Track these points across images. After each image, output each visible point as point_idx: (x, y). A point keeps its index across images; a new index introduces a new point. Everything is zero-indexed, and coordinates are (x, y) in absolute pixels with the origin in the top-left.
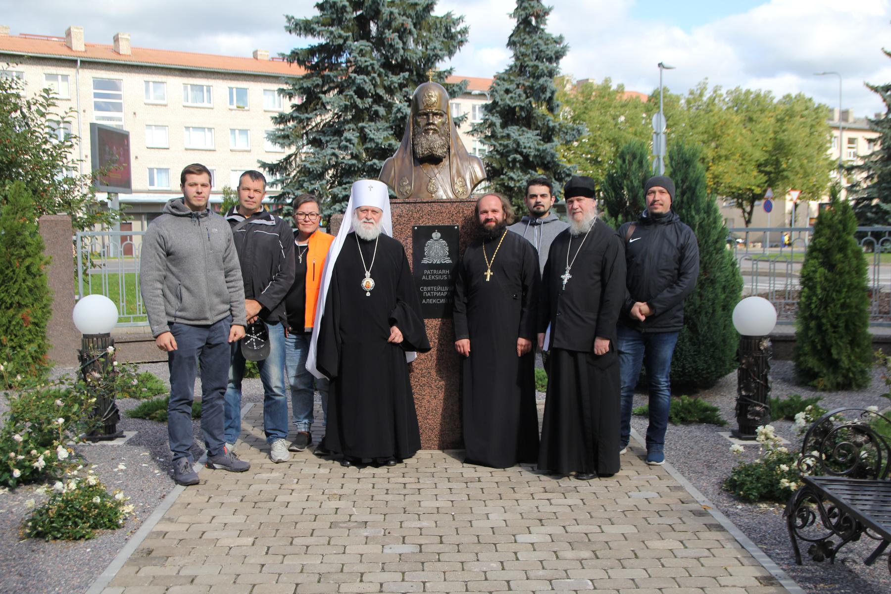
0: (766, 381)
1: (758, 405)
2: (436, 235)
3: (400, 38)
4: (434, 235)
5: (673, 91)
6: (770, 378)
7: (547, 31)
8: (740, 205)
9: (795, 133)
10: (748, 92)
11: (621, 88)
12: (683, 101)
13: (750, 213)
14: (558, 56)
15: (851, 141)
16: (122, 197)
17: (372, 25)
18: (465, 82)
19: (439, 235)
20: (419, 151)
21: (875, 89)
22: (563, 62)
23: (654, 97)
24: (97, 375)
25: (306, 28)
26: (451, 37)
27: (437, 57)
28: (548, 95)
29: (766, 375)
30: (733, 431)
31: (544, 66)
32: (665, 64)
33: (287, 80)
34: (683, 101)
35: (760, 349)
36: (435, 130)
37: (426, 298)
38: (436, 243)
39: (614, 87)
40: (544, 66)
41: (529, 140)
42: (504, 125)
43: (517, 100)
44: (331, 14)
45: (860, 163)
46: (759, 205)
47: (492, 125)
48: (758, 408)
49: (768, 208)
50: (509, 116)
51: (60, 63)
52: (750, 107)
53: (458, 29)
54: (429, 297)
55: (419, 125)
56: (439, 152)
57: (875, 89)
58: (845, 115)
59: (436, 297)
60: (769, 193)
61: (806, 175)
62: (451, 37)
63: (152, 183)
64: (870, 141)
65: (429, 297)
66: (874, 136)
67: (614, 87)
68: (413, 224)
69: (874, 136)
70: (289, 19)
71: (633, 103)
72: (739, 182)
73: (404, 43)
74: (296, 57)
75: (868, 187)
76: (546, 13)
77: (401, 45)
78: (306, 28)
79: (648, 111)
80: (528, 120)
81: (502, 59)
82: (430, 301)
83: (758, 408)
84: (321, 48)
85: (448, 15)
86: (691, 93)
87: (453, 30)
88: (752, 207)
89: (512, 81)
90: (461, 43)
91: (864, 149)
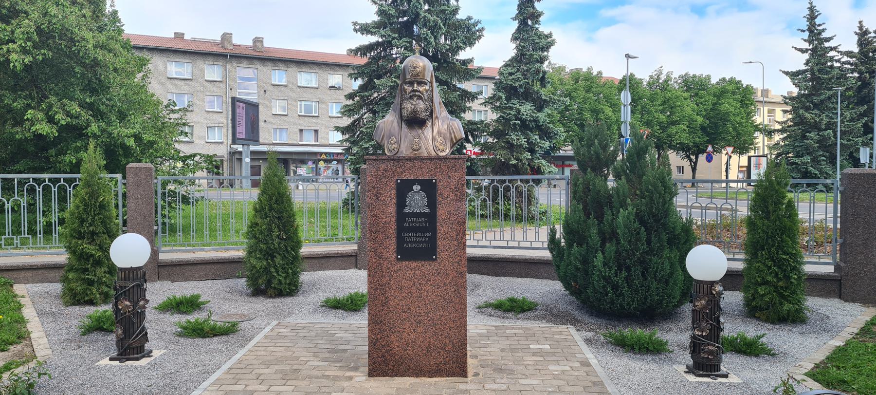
0: (719, 322)
1: (712, 345)
2: (416, 188)
3: (432, 33)
4: (414, 187)
5: (638, 76)
6: (722, 320)
7: (540, 30)
8: (688, 157)
9: (728, 106)
10: (694, 76)
11: (600, 73)
12: (645, 83)
13: (695, 163)
14: (547, 48)
15: (770, 111)
16: (253, 148)
17: (415, 27)
18: (480, 69)
19: (419, 187)
20: (405, 113)
21: (787, 73)
22: (552, 50)
23: (623, 81)
24: (128, 303)
25: (365, 29)
26: (469, 33)
27: (459, 48)
28: (541, 75)
29: (719, 317)
30: (687, 367)
31: (537, 55)
32: (631, 54)
33: (355, 67)
34: (645, 83)
35: (712, 293)
36: (419, 96)
37: (407, 242)
38: (417, 194)
39: (595, 73)
40: (537, 55)
41: (526, 109)
42: (508, 99)
43: (518, 80)
44: (385, 21)
45: (778, 127)
46: (702, 158)
47: (500, 98)
48: (711, 348)
49: (709, 159)
50: (511, 92)
51: (196, 57)
52: (694, 86)
53: (477, 28)
54: (410, 242)
55: (406, 92)
56: (423, 115)
57: (787, 73)
58: (765, 92)
59: (416, 242)
60: (710, 149)
61: (738, 135)
62: (469, 33)
63: (316, 140)
64: (785, 112)
65: (410, 242)
66: (789, 108)
67: (595, 73)
68: (396, 177)
69: (789, 108)
70: (355, 24)
71: (610, 82)
72: (685, 138)
73: (435, 38)
74: (363, 50)
75: (785, 145)
76: (539, 16)
77: (432, 40)
78: (365, 29)
79: (620, 90)
80: (527, 95)
81: (510, 51)
82: (410, 245)
83: (711, 348)
84: (378, 44)
85: (469, 18)
86: (651, 77)
87: (473, 30)
88: (697, 158)
89: (514, 67)
90: (479, 37)
91: (780, 116)
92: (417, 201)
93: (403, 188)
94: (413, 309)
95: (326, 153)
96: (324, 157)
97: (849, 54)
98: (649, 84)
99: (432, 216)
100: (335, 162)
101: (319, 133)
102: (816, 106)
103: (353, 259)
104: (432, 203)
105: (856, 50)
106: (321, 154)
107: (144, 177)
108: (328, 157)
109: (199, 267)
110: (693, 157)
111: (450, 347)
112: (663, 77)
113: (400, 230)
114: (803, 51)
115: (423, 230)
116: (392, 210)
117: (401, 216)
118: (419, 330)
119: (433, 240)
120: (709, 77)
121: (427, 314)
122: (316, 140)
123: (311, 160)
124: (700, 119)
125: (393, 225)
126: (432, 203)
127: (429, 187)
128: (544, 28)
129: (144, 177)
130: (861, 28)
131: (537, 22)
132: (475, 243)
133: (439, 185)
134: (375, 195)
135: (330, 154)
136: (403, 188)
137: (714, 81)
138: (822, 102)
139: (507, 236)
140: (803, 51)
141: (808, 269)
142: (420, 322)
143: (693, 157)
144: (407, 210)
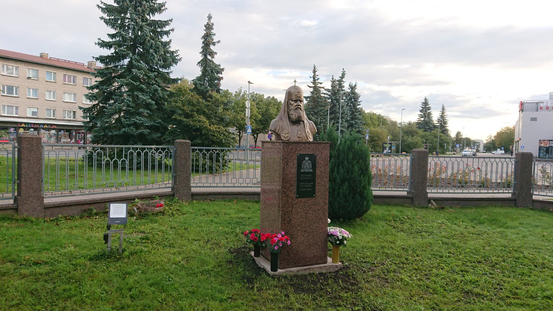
2: (307, 158)
13: (257, 138)
25: (103, 44)
63: (74, 117)
68: (297, 153)
74: (102, 59)
78: (103, 44)
81: (198, 72)
92: (307, 165)
93: (300, 159)
94: (303, 224)
95: (25, 123)
96: (23, 125)
97: (328, 90)
98: (235, 95)
99: (314, 174)
100: (33, 130)
101: (19, 109)
102: (316, 114)
103: (514, 202)
104: (314, 167)
105: (330, 88)
106: (21, 123)
107: (35, 144)
108: (27, 126)
109: (73, 207)
110: (255, 135)
111: (320, 243)
112: (242, 93)
113: (299, 181)
114: (310, 87)
115: (309, 181)
116: (294, 170)
117: (299, 174)
118: (306, 235)
119: (314, 186)
120: (263, 95)
121: (310, 226)
122: (74, 117)
123: (63, 129)
124: (260, 116)
125: (295, 178)
126: (314, 167)
127: (313, 158)
128: (217, 60)
129: (35, 144)
130: (333, 79)
131: (213, 57)
132: (195, 185)
133: (317, 157)
134: (286, 163)
135: (28, 123)
136: (300, 159)
137: (265, 97)
138: (318, 112)
139: (204, 181)
140: (310, 87)
141: (374, 193)
142: (306, 231)
143: (255, 135)
144: (302, 171)
